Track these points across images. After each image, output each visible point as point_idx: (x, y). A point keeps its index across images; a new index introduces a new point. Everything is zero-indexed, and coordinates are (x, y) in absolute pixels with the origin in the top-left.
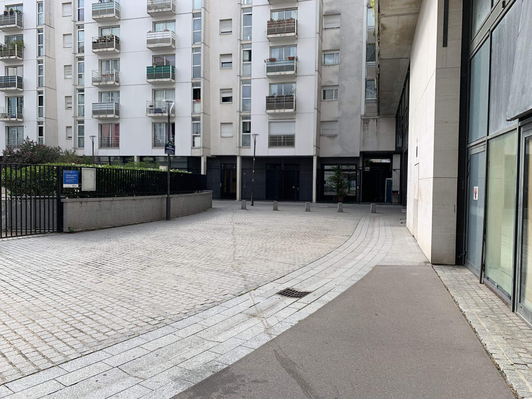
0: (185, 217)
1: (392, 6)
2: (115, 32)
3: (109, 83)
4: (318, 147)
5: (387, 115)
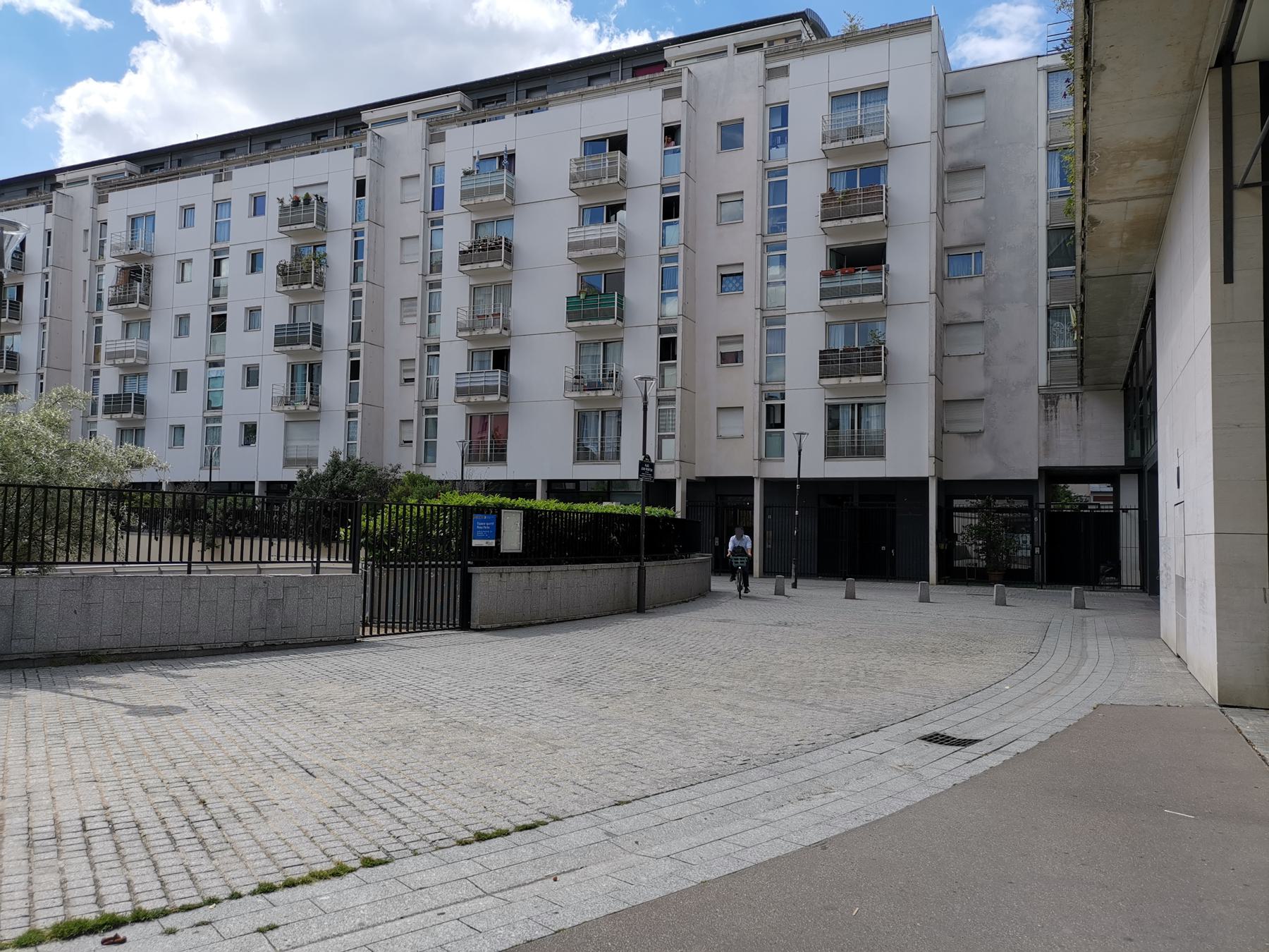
0: (668, 608)
1: (1111, 185)
2: (503, 232)
3: (489, 332)
4: (938, 459)
5: (1101, 387)
